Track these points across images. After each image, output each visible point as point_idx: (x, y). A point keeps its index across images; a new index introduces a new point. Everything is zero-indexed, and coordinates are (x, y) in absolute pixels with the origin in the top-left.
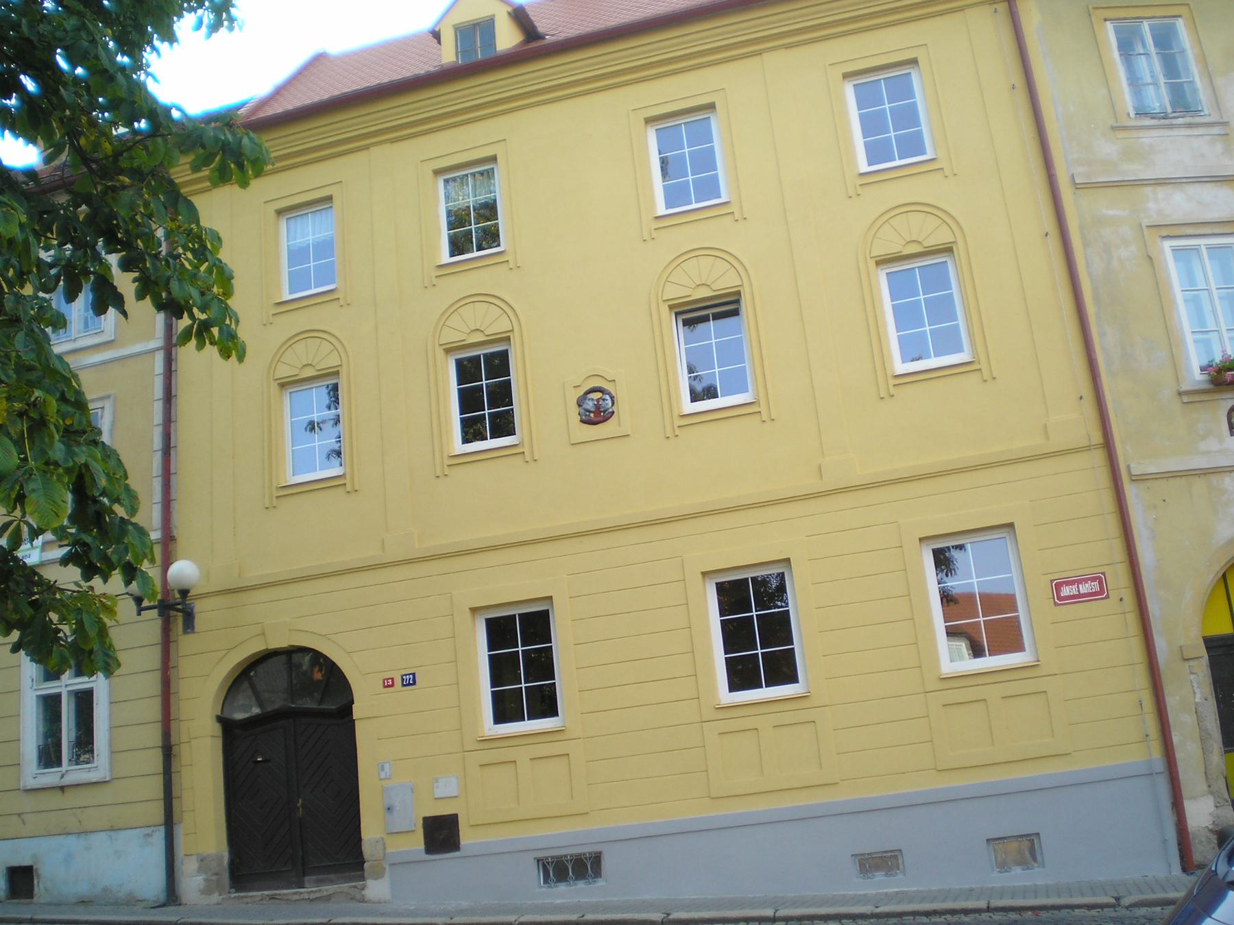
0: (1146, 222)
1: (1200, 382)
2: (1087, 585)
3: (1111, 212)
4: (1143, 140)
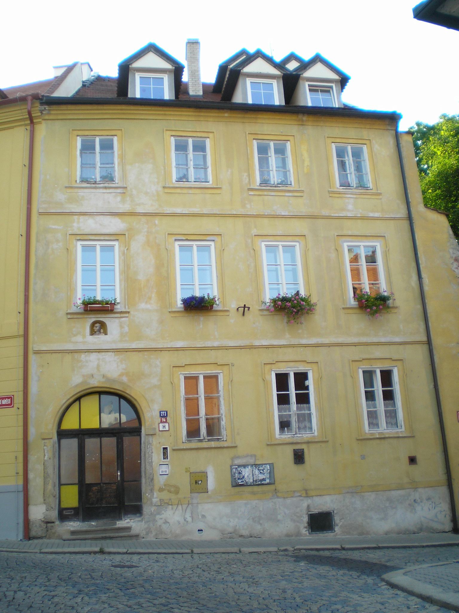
0: (70, 232)
1: (180, 308)
2: (5, 400)
3: (53, 227)
4: (79, 193)
